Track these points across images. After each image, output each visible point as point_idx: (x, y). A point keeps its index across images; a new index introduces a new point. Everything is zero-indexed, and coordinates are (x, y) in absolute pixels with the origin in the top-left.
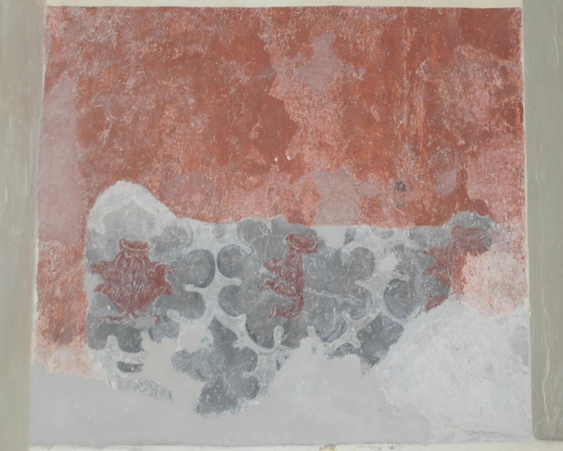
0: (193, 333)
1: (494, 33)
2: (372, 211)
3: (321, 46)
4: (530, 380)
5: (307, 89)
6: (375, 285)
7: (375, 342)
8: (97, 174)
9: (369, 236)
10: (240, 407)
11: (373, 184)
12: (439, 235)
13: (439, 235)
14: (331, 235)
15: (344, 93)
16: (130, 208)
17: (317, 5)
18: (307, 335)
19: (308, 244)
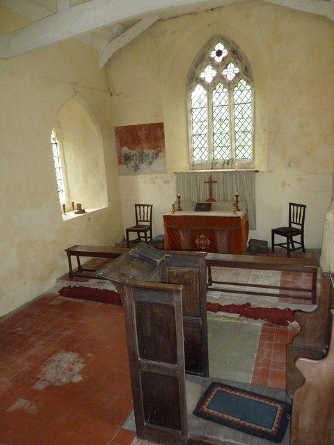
0: (133, 163)
1: (305, 207)
2: (149, 148)
3: (143, 129)
4: (196, 404)
5: (142, 134)
6: (150, 157)
7: (151, 163)
8: (122, 146)
9: (149, 151)
10: (189, 71)
11: (149, 145)
12: (156, 151)
13: (156, 151)
14: (145, 151)
15: (145, 134)
16: (125, 150)
17: (154, 122)
18: (161, 126)
19: (143, 152)
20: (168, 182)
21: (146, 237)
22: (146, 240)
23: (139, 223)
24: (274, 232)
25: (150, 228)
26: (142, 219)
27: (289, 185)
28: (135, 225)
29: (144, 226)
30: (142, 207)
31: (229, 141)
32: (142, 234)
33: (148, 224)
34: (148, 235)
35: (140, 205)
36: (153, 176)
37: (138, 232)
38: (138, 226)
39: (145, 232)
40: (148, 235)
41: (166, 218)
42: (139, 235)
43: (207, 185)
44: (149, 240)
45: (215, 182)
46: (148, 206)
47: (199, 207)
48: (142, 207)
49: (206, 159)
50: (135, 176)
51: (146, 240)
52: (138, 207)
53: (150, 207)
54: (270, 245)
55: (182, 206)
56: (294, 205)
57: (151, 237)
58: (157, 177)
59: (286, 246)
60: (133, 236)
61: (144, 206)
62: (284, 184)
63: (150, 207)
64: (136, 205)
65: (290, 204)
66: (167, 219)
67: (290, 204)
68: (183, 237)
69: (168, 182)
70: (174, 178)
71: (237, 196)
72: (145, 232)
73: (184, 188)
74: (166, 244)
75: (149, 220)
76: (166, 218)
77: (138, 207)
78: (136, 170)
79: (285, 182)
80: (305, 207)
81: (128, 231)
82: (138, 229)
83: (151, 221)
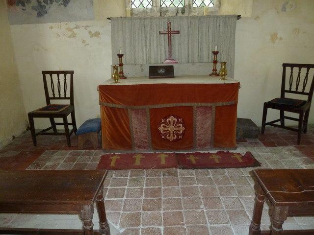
1: (72, 73)
20: (97, 34)
21: (66, 124)
22: (67, 128)
23: (53, 102)
24: (267, 105)
25: (71, 109)
26: (57, 96)
27: (281, 39)
28: (44, 105)
29: (62, 106)
30: (55, 76)
31: (151, 3)
32: (60, 120)
33: (68, 102)
34: (69, 120)
35: (51, 73)
36: (72, 25)
37: (52, 117)
38: (49, 107)
39: (64, 116)
40: (69, 120)
41: (103, 89)
42: (52, 122)
43: (164, 38)
44: (71, 128)
45: (178, 32)
46: (65, 73)
47: (154, 71)
48: (62, 76)
49: (150, 7)
50: (40, 25)
51: (67, 128)
52: (48, 76)
53: (68, 76)
54: (259, 123)
55: (126, 70)
56: (292, 66)
57: (74, 123)
58: (77, 27)
59: (279, 123)
60: (43, 124)
61: (58, 73)
62: (274, 37)
63: (68, 76)
64: (44, 73)
65: (285, 65)
66: (105, 90)
67: (285, 65)
68: (138, 125)
69: (97, 34)
70: (108, 27)
71: (216, 53)
72: (64, 116)
73: (124, 42)
74: (106, 133)
75: (68, 95)
76: (103, 89)
77: (48, 76)
78: (40, 15)
79: (277, 34)
80: (72, 73)
81: (32, 116)
82: (50, 111)
83: (72, 98)
